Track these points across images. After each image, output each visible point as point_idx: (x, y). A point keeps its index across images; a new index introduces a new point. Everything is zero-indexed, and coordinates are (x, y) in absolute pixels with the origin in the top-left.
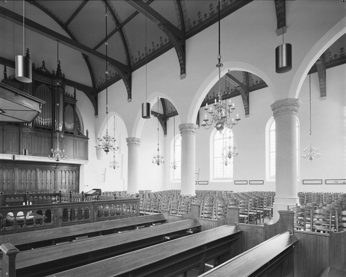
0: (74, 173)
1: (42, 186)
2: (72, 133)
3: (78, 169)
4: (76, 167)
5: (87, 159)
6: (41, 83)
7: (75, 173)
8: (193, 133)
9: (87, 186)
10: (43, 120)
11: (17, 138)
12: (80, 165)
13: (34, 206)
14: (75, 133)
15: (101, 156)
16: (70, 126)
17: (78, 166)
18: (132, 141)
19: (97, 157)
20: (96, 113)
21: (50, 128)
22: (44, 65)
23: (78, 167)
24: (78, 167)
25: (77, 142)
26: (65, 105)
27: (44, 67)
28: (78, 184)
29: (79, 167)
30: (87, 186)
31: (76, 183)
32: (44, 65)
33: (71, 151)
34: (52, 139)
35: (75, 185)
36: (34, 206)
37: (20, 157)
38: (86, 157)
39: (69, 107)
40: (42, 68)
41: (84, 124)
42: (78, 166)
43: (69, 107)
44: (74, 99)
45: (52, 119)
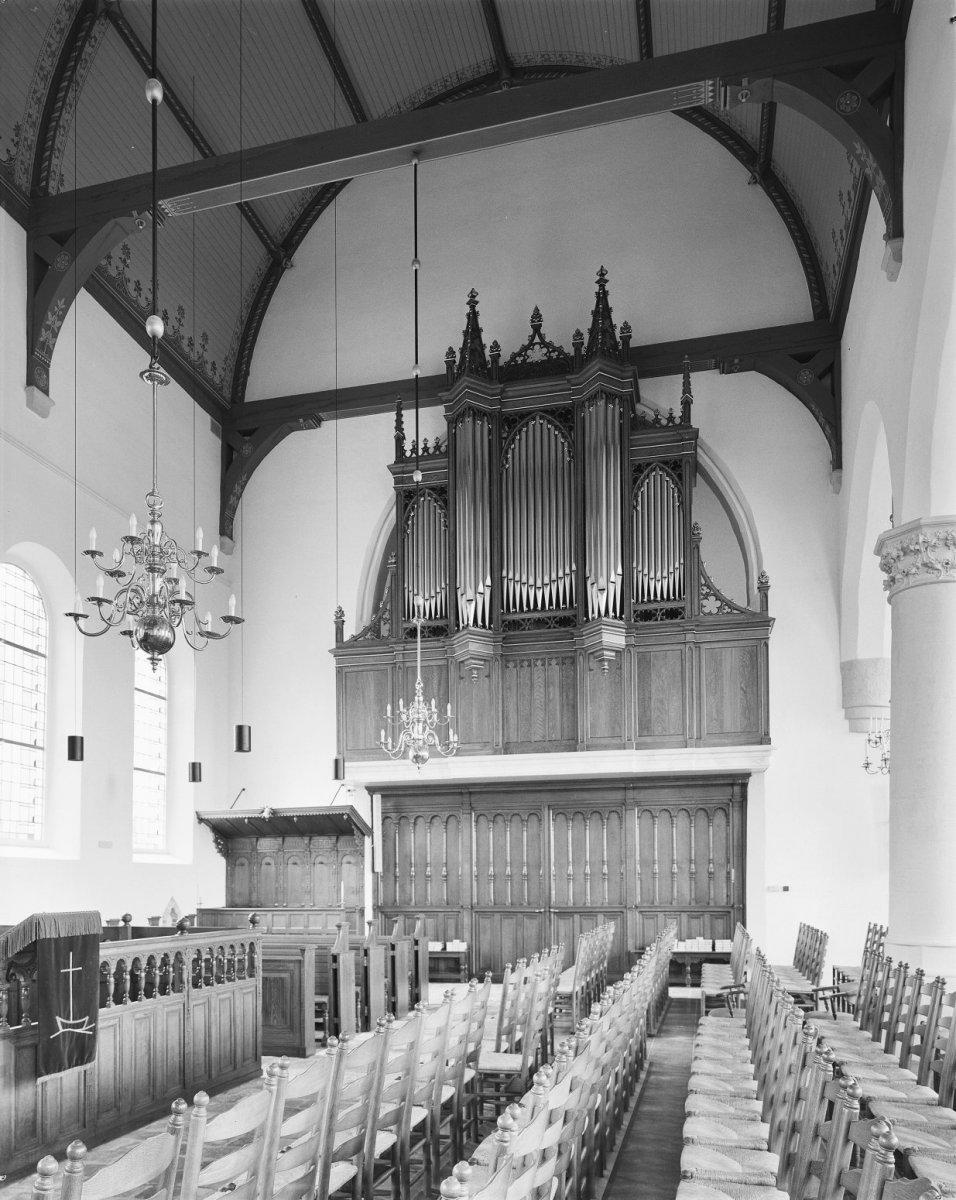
0: (719, 818)
1: (426, 891)
2: (673, 614)
3: (738, 798)
4: (728, 790)
5: (764, 739)
6: (525, 416)
7: (724, 822)
8: (931, 577)
9: (786, 889)
10: (652, 575)
11: (439, 690)
12: (748, 775)
13: (58, 979)
14: (688, 608)
15: (869, 712)
16: (659, 579)
17: (735, 786)
18: (905, 551)
19: (848, 717)
20: (837, 463)
21: (567, 613)
22: (537, 329)
23: (737, 789)
24: (737, 789)
25: (703, 652)
26: (634, 476)
27: (537, 340)
28: (737, 877)
29: (744, 786)
30: (786, 889)
31: (729, 873)
32: (537, 329)
33: (420, 712)
34: (574, 662)
35: (724, 885)
36: (58, 979)
37: (447, 763)
38: (759, 735)
39: (657, 486)
40: (531, 344)
41: (763, 549)
42: (735, 786)
43: (657, 486)
44: (683, 429)
45: (574, 567)
